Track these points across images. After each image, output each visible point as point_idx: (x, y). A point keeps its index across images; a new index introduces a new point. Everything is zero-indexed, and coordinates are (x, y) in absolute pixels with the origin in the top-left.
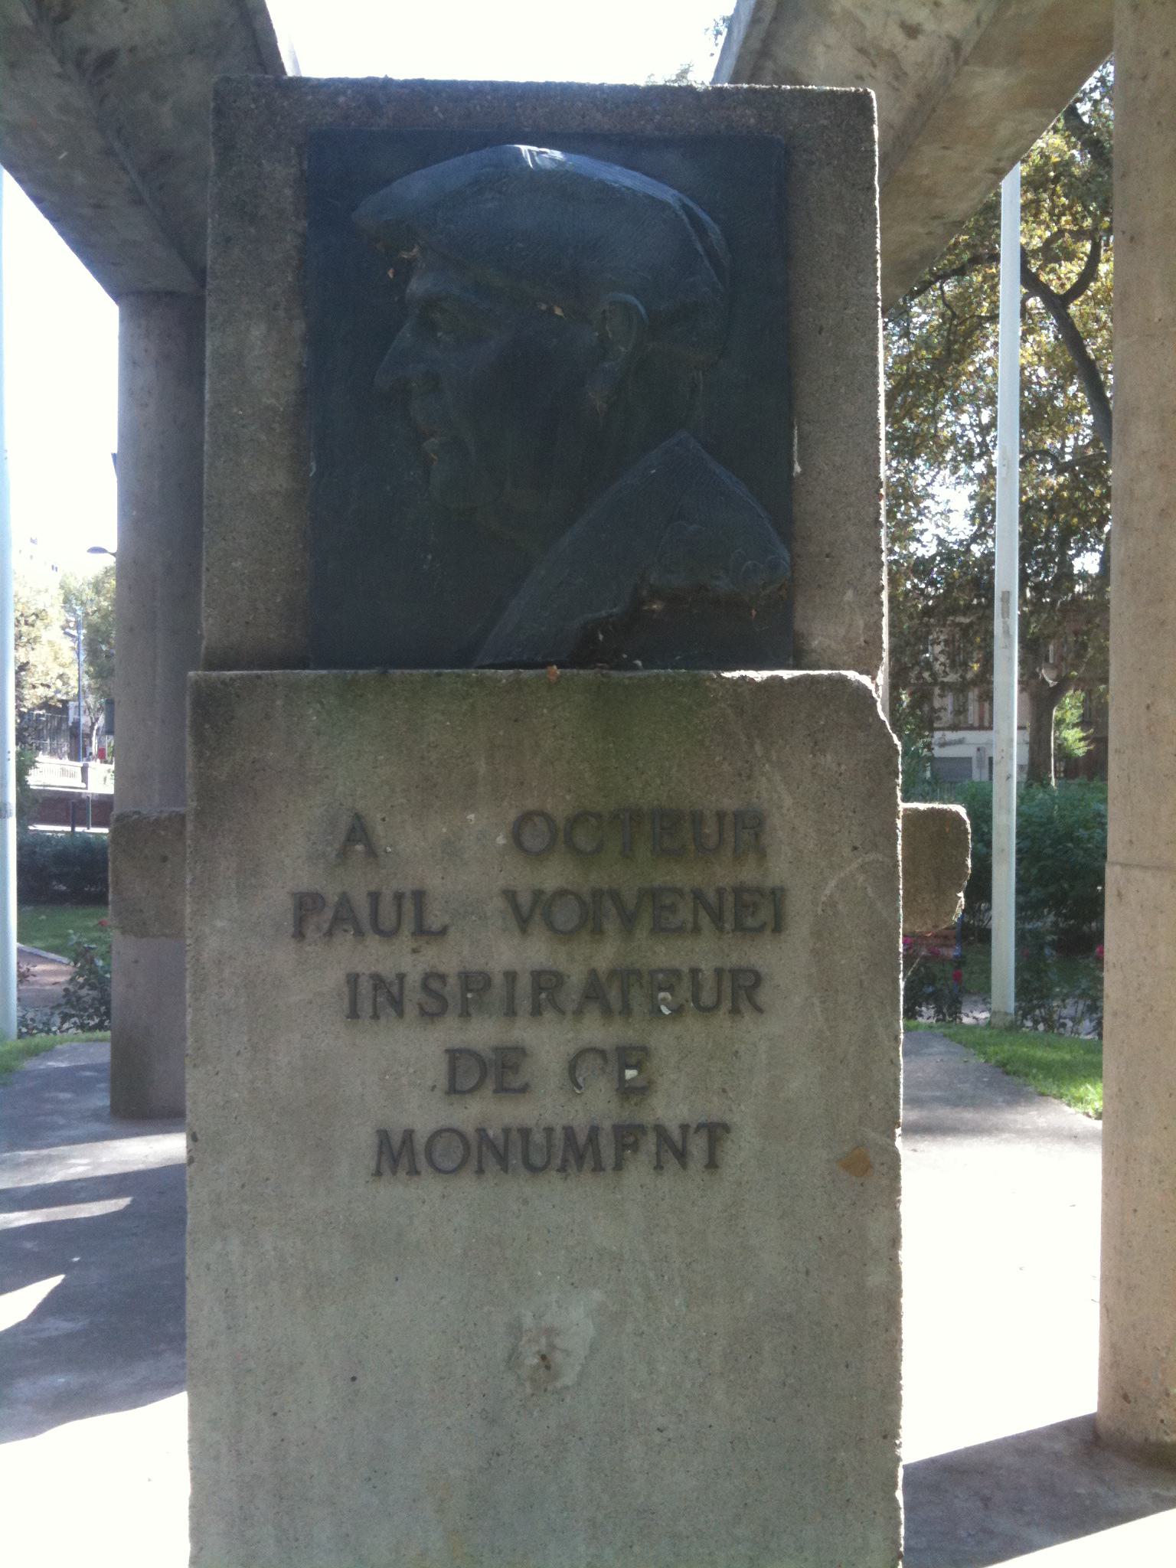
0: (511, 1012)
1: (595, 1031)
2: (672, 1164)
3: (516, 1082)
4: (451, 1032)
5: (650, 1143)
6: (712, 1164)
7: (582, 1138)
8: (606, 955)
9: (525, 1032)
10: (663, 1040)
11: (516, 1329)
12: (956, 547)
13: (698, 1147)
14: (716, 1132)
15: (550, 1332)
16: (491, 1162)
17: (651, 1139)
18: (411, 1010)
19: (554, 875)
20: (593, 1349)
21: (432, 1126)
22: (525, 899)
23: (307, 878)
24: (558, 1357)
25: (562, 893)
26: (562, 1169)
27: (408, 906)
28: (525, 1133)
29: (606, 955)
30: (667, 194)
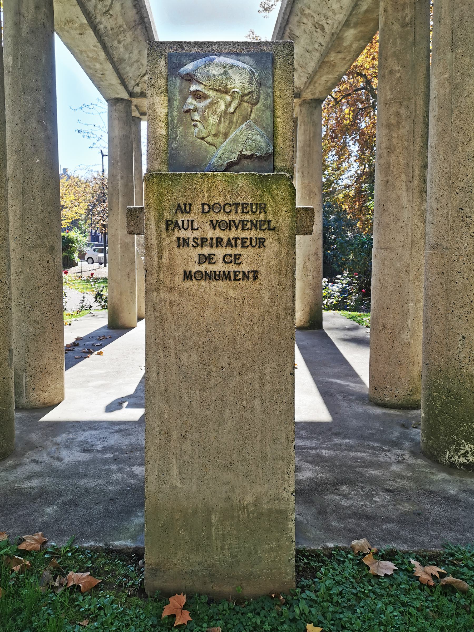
9: (214, 251)
21: (196, 270)
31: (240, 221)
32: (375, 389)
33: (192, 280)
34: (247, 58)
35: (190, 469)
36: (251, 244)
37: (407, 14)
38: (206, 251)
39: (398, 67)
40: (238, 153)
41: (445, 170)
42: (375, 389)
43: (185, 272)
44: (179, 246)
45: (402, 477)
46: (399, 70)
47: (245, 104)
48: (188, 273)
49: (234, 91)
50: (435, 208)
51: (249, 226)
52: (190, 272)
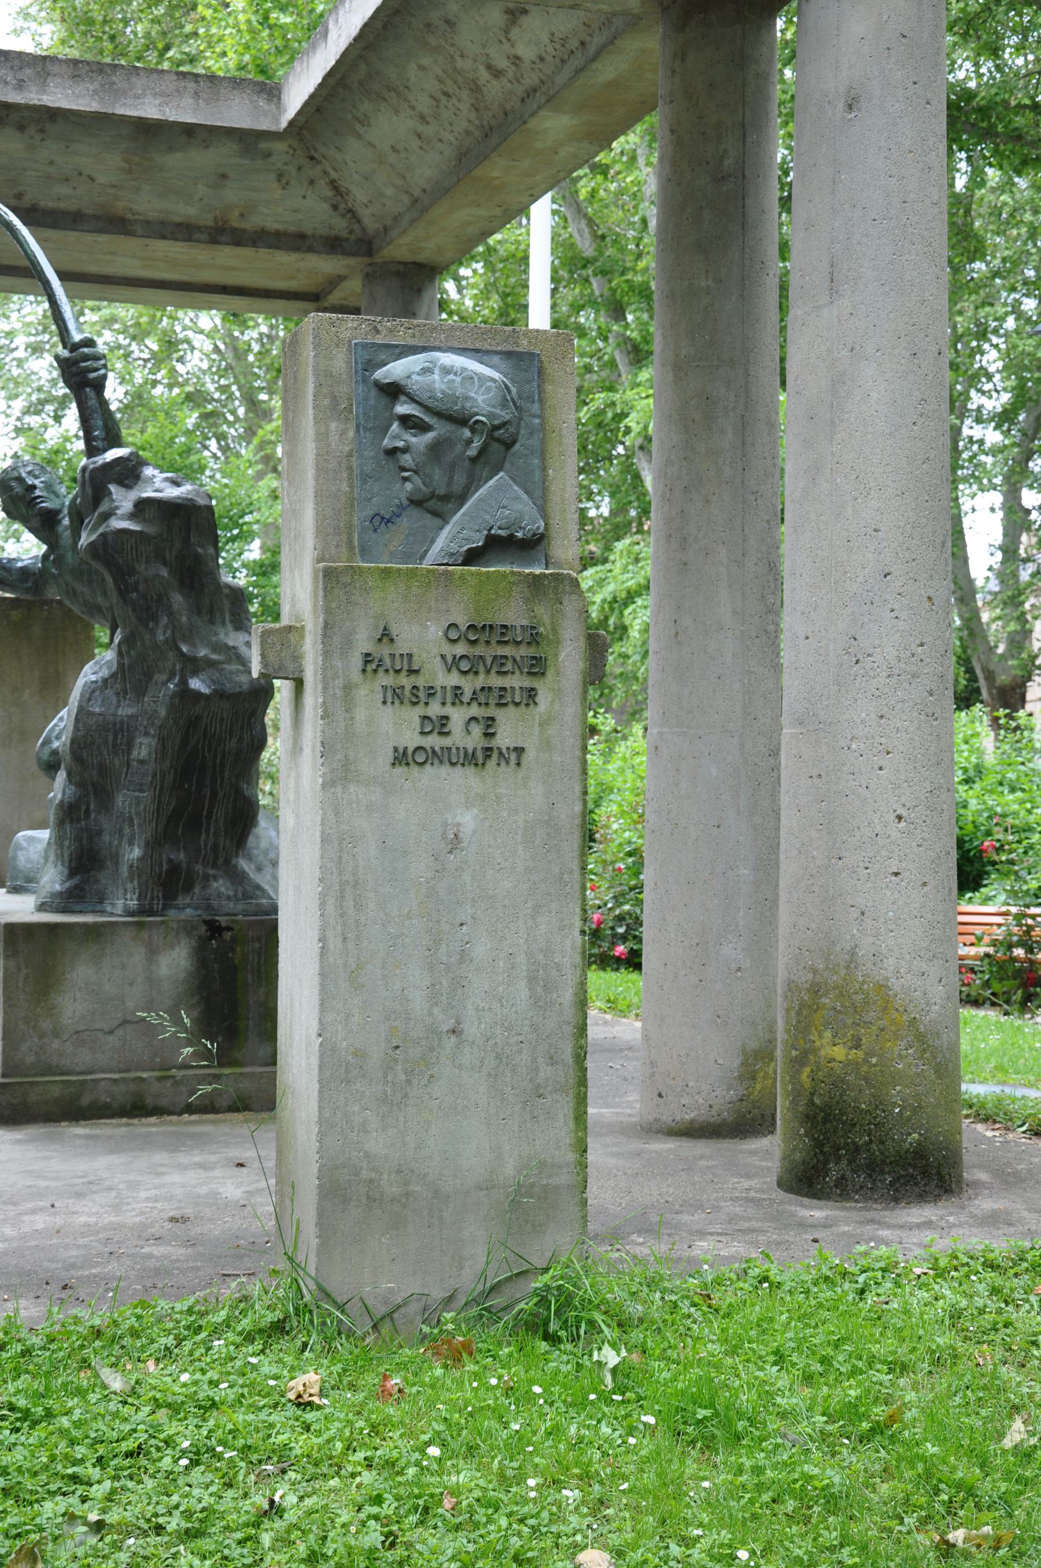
0: (444, 704)
1: (475, 710)
2: (503, 763)
3: (446, 730)
4: (389, 680)
5: (495, 755)
6: (518, 764)
7: (470, 751)
8: (480, 681)
9: (448, 710)
10: (500, 714)
11: (445, 824)
12: (136, 882)
13: (513, 756)
14: (520, 751)
15: (459, 825)
16: (436, 761)
17: (496, 752)
18: (406, 701)
19: (461, 649)
20: (474, 832)
21: (416, 745)
22: (450, 660)
23: (366, 647)
24: (461, 835)
25: (462, 657)
26: (463, 765)
27: (221, 861)
28: (449, 749)
29: (480, 681)
30: (496, 375)
31: (495, 657)
32: (660, 1095)
33: (408, 764)
34: (496, 359)
35: (402, 1119)
36: (513, 697)
37: (725, 151)
38: (435, 709)
39: (707, 279)
40: (485, 532)
41: (819, 552)
42: (660, 1095)
43: (396, 749)
44: (384, 702)
45: (742, 1218)
46: (708, 287)
47: (495, 445)
48: (401, 751)
49: (477, 422)
50: (802, 635)
51: (509, 667)
52: (406, 749)
